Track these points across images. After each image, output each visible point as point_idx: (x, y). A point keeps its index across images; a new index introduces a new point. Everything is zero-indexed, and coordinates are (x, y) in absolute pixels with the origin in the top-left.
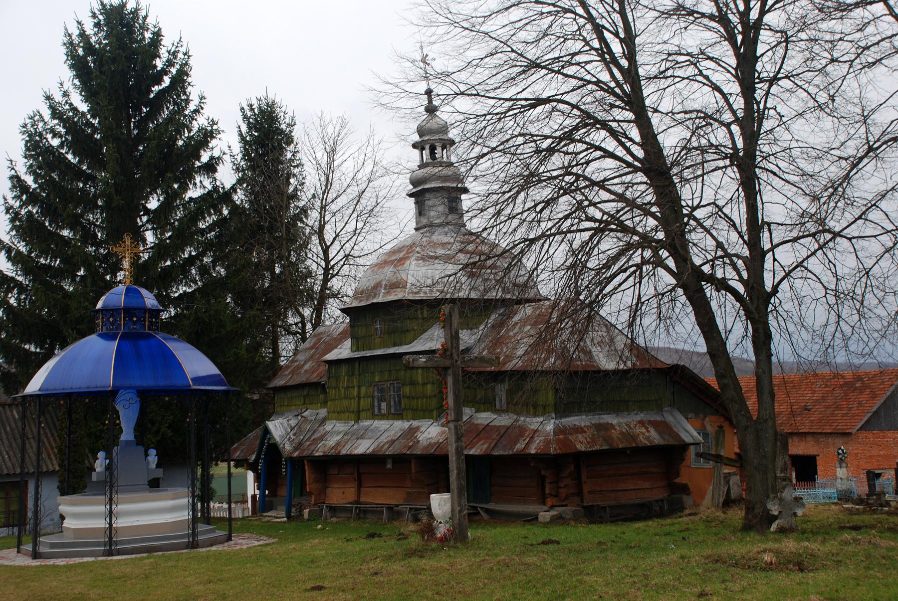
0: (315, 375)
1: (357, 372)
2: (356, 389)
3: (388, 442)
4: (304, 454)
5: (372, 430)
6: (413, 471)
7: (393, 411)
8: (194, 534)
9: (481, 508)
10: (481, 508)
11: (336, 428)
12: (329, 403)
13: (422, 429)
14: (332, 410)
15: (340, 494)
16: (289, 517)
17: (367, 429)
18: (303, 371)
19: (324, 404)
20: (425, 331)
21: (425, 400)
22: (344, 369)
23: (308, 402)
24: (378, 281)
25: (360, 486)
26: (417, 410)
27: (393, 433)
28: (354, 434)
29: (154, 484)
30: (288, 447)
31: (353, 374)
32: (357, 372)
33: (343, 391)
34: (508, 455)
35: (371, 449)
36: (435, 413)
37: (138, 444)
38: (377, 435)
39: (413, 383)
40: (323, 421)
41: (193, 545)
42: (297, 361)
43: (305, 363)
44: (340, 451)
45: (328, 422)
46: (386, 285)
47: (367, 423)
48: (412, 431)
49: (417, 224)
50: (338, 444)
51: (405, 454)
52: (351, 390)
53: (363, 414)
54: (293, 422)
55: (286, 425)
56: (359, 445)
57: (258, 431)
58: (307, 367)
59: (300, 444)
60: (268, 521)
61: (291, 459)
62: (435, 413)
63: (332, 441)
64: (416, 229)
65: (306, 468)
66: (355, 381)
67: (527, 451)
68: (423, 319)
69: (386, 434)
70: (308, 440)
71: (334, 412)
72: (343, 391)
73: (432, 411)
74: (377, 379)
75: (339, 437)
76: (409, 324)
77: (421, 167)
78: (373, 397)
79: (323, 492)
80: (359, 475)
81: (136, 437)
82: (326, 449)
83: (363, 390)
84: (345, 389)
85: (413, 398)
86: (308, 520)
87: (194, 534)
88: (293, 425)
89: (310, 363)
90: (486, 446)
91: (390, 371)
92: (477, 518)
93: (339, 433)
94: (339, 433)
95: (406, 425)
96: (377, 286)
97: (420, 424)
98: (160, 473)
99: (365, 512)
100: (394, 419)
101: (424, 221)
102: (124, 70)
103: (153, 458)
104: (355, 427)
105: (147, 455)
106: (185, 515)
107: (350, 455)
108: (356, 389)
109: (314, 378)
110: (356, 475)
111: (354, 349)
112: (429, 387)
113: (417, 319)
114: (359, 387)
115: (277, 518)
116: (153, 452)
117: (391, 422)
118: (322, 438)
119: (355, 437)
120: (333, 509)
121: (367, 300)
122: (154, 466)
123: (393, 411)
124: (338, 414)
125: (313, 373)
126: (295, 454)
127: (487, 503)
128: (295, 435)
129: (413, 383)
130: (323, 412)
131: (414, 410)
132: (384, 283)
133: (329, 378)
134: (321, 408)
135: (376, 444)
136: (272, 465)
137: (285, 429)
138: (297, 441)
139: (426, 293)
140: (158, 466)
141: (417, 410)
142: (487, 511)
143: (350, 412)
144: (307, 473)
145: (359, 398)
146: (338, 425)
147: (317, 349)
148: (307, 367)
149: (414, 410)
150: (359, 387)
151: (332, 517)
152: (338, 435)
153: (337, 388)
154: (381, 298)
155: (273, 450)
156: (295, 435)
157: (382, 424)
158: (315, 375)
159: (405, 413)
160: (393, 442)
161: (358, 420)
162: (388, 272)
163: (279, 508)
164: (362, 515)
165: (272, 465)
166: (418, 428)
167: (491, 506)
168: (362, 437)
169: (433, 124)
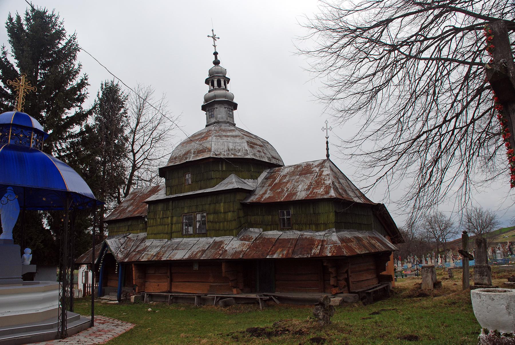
1: (170, 208)
2: (170, 218)
3: (200, 251)
4: (133, 260)
5: (183, 244)
6: (224, 270)
8: (64, 322)
9: (273, 296)
10: (273, 296)
12: (148, 229)
14: (150, 233)
15: (156, 286)
16: (119, 300)
17: (179, 244)
18: (127, 212)
19: (144, 229)
22: (160, 207)
23: (130, 230)
25: (171, 281)
26: (219, 230)
27: (201, 245)
29: (28, 277)
30: (120, 256)
32: (170, 208)
33: (159, 220)
34: (307, 258)
37: (15, 242)
38: (187, 247)
39: (216, 212)
40: (143, 240)
41: (62, 335)
42: (122, 207)
43: (128, 207)
46: (195, 152)
48: (218, 245)
49: (207, 123)
50: (158, 253)
51: (218, 259)
53: (174, 235)
54: (122, 241)
55: (118, 242)
57: (99, 248)
58: (129, 209)
60: (106, 303)
61: (122, 264)
62: (235, 231)
63: (154, 252)
64: (207, 126)
65: (134, 269)
68: (223, 171)
70: (134, 251)
72: (159, 220)
73: (232, 230)
74: (186, 211)
75: (158, 249)
76: (213, 174)
77: (209, 92)
78: (182, 223)
79: (143, 284)
80: (171, 274)
81: (13, 237)
82: (149, 256)
83: (175, 219)
84: (161, 219)
85: (216, 222)
86: (134, 303)
87: (64, 322)
88: (122, 243)
90: (285, 252)
91: (197, 206)
92: (272, 303)
93: (157, 247)
94: (157, 247)
96: (189, 152)
98: (33, 269)
99: (176, 298)
101: (213, 120)
103: (28, 255)
105: (23, 253)
106: (56, 305)
108: (170, 218)
110: (169, 274)
111: (168, 193)
113: (219, 171)
114: (172, 217)
115: (111, 300)
116: (28, 251)
117: (197, 239)
118: (144, 250)
119: (170, 249)
120: (151, 296)
121: (180, 162)
122: (29, 263)
124: (156, 235)
125: (134, 212)
126: (126, 260)
127: (274, 292)
128: (124, 248)
129: (216, 212)
130: (142, 235)
131: (216, 230)
133: (149, 213)
134: (140, 232)
136: (107, 268)
137: (118, 245)
138: (125, 252)
139: (224, 155)
140: (32, 262)
141: (219, 230)
142: (279, 298)
143: (164, 233)
144: (134, 272)
146: (155, 242)
147: (135, 200)
148: (129, 209)
149: (216, 230)
150: (172, 217)
151: (150, 301)
152: (153, 248)
153: (154, 219)
154: (192, 158)
155: (110, 258)
157: (192, 240)
160: (204, 251)
161: (170, 238)
162: (195, 146)
163: (110, 293)
164: (174, 300)
165: (107, 268)
167: (277, 294)
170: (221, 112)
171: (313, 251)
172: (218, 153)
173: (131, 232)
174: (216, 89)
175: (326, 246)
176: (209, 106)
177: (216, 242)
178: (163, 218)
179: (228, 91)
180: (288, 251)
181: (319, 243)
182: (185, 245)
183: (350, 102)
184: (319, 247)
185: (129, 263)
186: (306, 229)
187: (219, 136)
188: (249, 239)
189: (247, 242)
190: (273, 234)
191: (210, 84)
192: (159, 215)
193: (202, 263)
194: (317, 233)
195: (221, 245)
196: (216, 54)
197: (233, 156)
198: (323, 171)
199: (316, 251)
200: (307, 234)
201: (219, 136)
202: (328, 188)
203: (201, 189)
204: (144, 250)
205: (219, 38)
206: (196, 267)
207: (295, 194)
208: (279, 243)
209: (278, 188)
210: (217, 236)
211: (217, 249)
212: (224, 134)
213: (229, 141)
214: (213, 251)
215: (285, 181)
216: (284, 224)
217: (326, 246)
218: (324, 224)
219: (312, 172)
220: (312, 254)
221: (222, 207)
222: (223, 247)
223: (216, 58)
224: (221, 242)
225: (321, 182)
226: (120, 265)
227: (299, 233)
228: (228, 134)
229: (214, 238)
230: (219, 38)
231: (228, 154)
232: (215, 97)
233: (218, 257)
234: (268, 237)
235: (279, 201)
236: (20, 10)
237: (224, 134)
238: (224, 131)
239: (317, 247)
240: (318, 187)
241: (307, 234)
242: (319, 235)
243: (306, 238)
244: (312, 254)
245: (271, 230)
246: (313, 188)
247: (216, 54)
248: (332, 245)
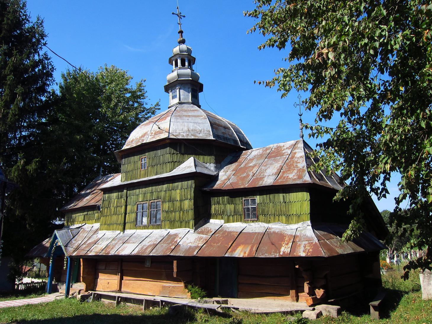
3: (150, 245)
5: (135, 237)
19: (98, 220)
28: (120, 240)
44: (109, 252)
56: (125, 248)
63: (102, 245)
67: (295, 254)
69: (148, 240)
71: (105, 224)
85: (172, 212)
102: (280, 50)
111: (123, 180)
119: (121, 242)
124: (109, 226)
126: (74, 254)
130: (97, 225)
134: (95, 222)
135: (140, 247)
139: (184, 136)
159: (163, 224)
171: (282, 249)
172: (177, 134)
173: (86, 222)
175: (299, 243)
177: (170, 236)
178: (117, 207)
180: (252, 248)
181: (290, 240)
182: (137, 238)
183: (298, 212)
184: (290, 244)
185: (78, 258)
186: (274, 221)
187: (179, 116)
188: (207, 232)
189: (204, 236)
190: (236, 226)
192: (114, 204)
193: (155, 260)
194: (288, 227)
195: (175, 238)
197: (193, 137)
198: (295, 153)
199: (285, 250)
200: (276, 227)
201: (179, 116)
202: (301, 171)
203: (157, 174)
204: (95, 243)
205: (184, 17)
206: (148, 264)
207: (262, 179)
208: (239, 237)
209: (243, 173)
210: (172, 228)
211: (169, 244)
212: (185, 114)
213: (189, 121)
214: (165, 245)
215: (251, 165)
216: (249, 215)
217: (299, 243)
218: (296, 215)
219: (283, 155)
220: (281, 253)
221: (177, 194)
222: (177, 241)
224: (176, 235)
225: (293, 165)
226: (69, 259)
227: (266, 225)
228: (190, 114)
229: (169, 230)
230: (184, 17)
231: (188, 135)
233: (168, 254)
234: (230, 230)
235: (242, 187)
236: (385, 321)
237: (185, 114)
238: (185, 111)
239: (287, 244)
240: (289, 171)
241: (276, 227)
242: (291, 228)
243: (274, 232)
244: (281, 253)
245: (233, 222)
246: (284, 172)
248: (307, 242)
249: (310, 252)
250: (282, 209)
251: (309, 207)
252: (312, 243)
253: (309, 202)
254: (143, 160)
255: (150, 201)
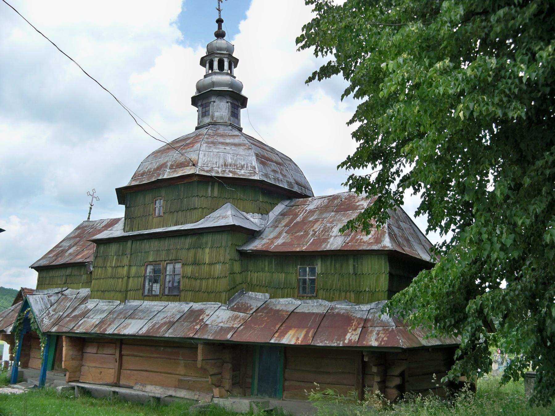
0: (80, 256)
1: (128, 251)
3: (165, 323)
4: (64, 330)
5: (142, 311)
7: (166, 293)
11: (99, 307)
13: (207, 312)
14: (96, 289)
17: (136, 309)
19: (87, 284)
20: (214, 210)
21: (211, 280)
22: (113, 248)
24: (162, 162)
26: (199, 291)
28: (121, 313)
31: (124, 254)
32: (128, 251)
33: (110, 270)
35: (144, 330)
36: (223, 295)
40: (85, 300)
43: (70, 247)
45: (89, 300)
47: (135, 303)
48: (194, 316)
49: (198, 124)
50: (102, 322)
52: (120, 270)
53: (130, 294)
59: (59, 319)
61: (48, 335)
62: (223, 295)
65: (64, 345)
66: (126, 261)
69: (161, 316)
72: (110, 270)
75: (103, 316)
80: (121, 356)
83: (133, 270)
85: (196, 279)
88: (53, 301)
89: (74, 248)
91: (168, 250)
95: (185, 307)
97: (203, 306)
100: (168, 300)
101: (207, 120)
104: (121, 306)
107: (119, 335)
108: (126, 268)
109: (79, 259)
112: (218, 267)
117: (164, 303)
118: (84, 315)
123: (166, 293)
124: (101, 293)
126: (54, 330)
130: (84, 292)
132: (169, 164)
133: (96, 257)
134: (82, 287)
135: (150, 324)
137: (45, 304)
138: (56, 316)
141: (199, 291)
145: (129, 277)
156: (54, 310)
157: (156, 305)
158: (80, 256)
160: (171, 324)
161: (124, 299)
166: (201, 312)
168: (131, 317)
169: (221, 43)
170: (221, 109)
174: (215, 73)
176: (202, 98)
179: (235, 77)
191: (207, 65)
196: (220, 21)
223: (220, 27)
232: (213, 84)
239: (355, 330)
247: (220, 21)
249: (384, 341)
250: (351, 283)
251: (387, 283)
252: (388, 329)
253: (388, 275)
254: (157, 202)
255: (165, 261)
